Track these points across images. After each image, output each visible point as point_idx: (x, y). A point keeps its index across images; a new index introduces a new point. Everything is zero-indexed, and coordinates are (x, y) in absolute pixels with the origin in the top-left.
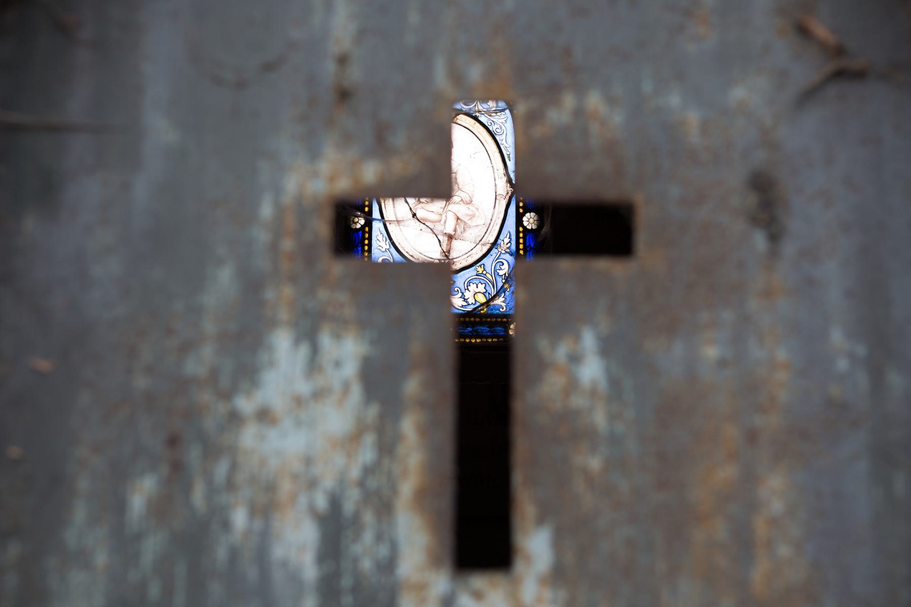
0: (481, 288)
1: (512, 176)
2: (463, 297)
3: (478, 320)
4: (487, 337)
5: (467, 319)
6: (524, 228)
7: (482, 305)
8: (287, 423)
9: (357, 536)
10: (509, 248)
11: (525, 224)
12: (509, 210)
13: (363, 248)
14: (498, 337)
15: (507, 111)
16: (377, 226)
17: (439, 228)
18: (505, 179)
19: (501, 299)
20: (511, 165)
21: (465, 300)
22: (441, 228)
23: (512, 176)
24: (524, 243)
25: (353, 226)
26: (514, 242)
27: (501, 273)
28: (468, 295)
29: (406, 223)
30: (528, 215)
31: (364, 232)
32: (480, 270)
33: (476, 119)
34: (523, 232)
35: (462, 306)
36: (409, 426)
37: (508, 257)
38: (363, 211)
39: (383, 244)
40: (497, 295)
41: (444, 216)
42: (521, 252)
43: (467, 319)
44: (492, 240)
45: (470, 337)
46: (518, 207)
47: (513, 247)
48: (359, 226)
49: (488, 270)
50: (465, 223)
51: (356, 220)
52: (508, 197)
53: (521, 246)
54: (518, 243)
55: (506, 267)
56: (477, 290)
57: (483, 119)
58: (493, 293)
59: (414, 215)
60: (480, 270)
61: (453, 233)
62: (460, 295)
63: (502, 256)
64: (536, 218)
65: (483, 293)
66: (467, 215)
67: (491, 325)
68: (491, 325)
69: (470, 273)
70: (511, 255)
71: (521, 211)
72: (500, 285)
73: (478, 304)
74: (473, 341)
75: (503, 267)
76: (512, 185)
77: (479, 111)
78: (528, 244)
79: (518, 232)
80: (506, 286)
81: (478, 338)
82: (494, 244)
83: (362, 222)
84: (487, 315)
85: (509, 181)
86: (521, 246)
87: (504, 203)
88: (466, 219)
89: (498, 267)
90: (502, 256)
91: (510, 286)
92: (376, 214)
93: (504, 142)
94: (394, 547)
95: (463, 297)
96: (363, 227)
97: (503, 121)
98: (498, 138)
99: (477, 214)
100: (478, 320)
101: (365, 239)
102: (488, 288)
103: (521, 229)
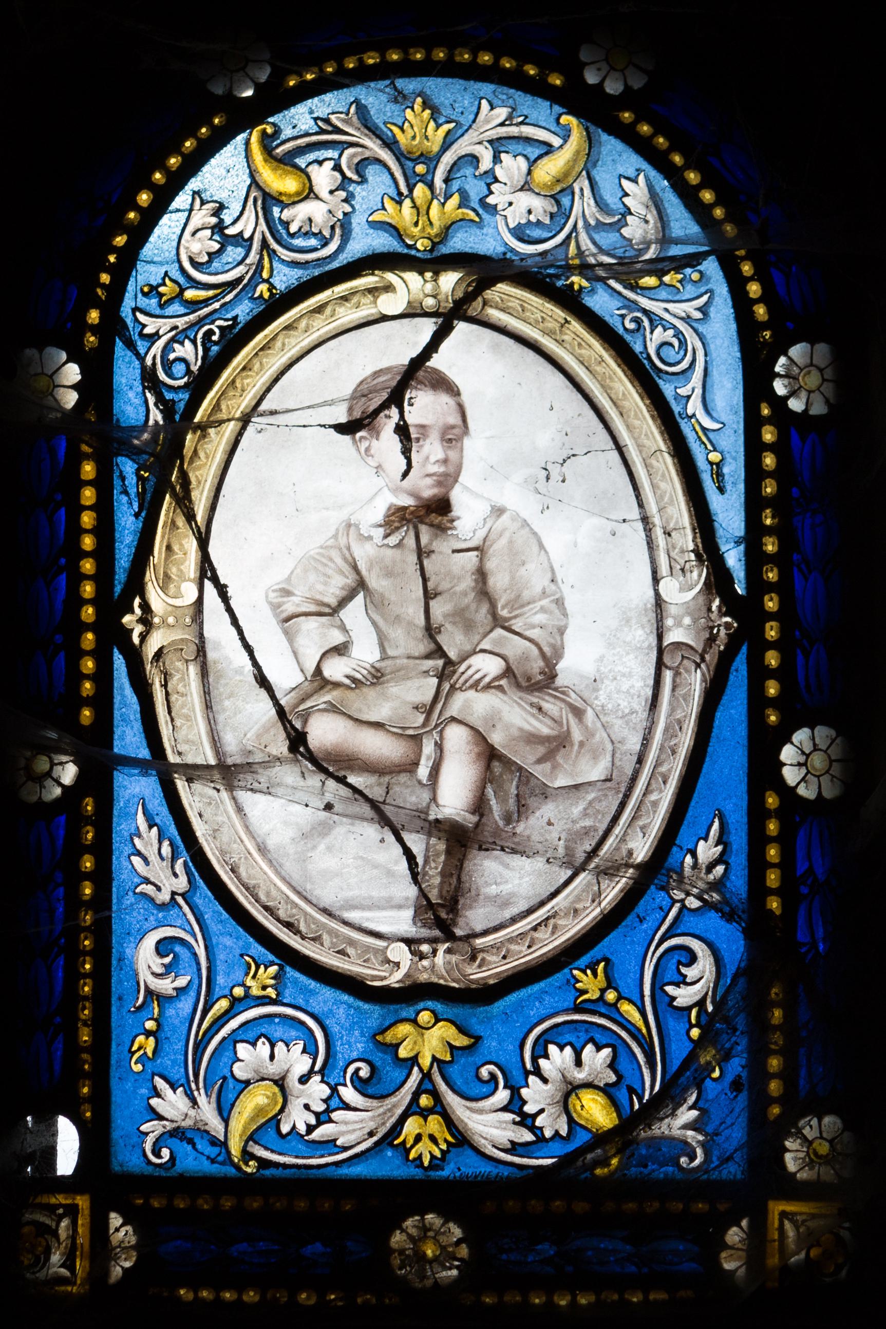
0: (596, 1060)
1: (734, 559)
2: (515, 1105)
3: (581, 1207)
5: (535, 1205)
6: (787, 793)
7: (601, 1139)
8: (427, 1132)
9: (742, 1107)
10: (717, 885)
11: (791, 775)
13: (76, 890)
15: (711, 266)
16: (135, 789)
17: (408, 796)
18: (698, 576)
19: (687, 1115)
21: (526, 1121)
22: (415, 798)
23: (734, 559)
24: (785, 865)
26: (739, 860)
27: (684, 996)
28: (536, 1095)
29: (264, 777)
30: (801, 736)
31: (78, 820)
33: (571, 302)
34: (779, 814)
35: (514, 1148)
37: (713, 922)
38: (70, 724)
39: (158, 871)
40: (668, 1098)
41: (428, 748)
42: (774, 904)
43: (535, 1205)
44: (641, 848)
45: (550, 1287)
46: (757, 702)
47: (739, 883)
50: (525, 777)
51: (42, 764)
52: (711, 657)
53: (773, 878)
54: (757, 865)
55: (703, 969)
56: (580, 1076)
57: (601, 302)
58: (651, 1084)
59: (298, 741)
60: (590, 984)
62: (502, 1096)
63: (691, 922)
64: (835, 752)
66: (532, 739)
69: (542, 1003)
70: (729, 916)
71: (89, 806)
72: (679, 1051)
73: (582, 1138)
75: (691, 973)
76: (731, 604)
77: (584, 269)
78: (801, 867)
79: (757, 814)
80: (706, 1057)
81: (585, 1289)
82: (656, 870)
83: (69, 773)
84: (619, 1186)
85: (719, 579)
86: (773, 878)
87: (696, 682)
88: (526, 757)
89: (671, 975)
90: (691, 922)
91: (725, 1057)
92: (129, 739)
93: (694, 406)
95: (515, 1105)
97: (690, 308)
99: (577, 735)
100: (581, 1207)
101: (77, 849)
103: (772, 801)
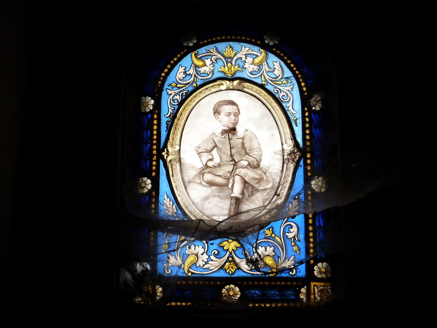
4: (276, 301)
6: (313, 191)
12: (297, 174)
14: (289, 301)
20: (298, 131)
23: (299, 139)
25: (141, 191)
27: (290, 235)
32: (269, 233)
36: (257, 212)
41: (231, 181)
45: (259, 302)
46: (306, 171)
48: (146, 191)
49: (277, 233)
50: (253, 187)
61: (240, 196)
65: (273, 257)
66: (255, 179)
67: (281, 289)
68: (281, 289)
74: (280, 305)
75: (292, 230)
87: (292, 166)
88: (253, 183)
89: (287, 230)
93: (290, 108)
94: (252, 185)
96: (150, 191)
97: (289, 88)
98: (284, 105)
99: (265, 178)
102: (276, 251)
